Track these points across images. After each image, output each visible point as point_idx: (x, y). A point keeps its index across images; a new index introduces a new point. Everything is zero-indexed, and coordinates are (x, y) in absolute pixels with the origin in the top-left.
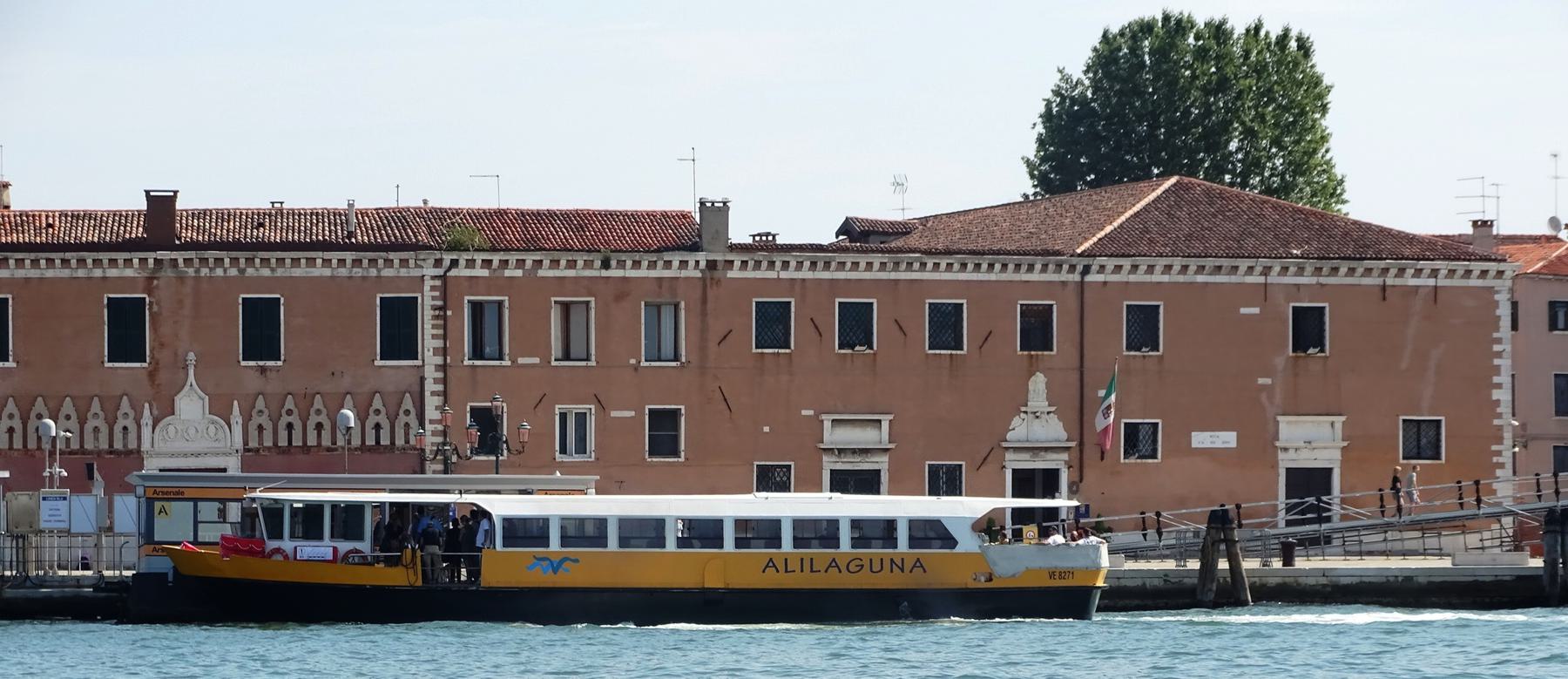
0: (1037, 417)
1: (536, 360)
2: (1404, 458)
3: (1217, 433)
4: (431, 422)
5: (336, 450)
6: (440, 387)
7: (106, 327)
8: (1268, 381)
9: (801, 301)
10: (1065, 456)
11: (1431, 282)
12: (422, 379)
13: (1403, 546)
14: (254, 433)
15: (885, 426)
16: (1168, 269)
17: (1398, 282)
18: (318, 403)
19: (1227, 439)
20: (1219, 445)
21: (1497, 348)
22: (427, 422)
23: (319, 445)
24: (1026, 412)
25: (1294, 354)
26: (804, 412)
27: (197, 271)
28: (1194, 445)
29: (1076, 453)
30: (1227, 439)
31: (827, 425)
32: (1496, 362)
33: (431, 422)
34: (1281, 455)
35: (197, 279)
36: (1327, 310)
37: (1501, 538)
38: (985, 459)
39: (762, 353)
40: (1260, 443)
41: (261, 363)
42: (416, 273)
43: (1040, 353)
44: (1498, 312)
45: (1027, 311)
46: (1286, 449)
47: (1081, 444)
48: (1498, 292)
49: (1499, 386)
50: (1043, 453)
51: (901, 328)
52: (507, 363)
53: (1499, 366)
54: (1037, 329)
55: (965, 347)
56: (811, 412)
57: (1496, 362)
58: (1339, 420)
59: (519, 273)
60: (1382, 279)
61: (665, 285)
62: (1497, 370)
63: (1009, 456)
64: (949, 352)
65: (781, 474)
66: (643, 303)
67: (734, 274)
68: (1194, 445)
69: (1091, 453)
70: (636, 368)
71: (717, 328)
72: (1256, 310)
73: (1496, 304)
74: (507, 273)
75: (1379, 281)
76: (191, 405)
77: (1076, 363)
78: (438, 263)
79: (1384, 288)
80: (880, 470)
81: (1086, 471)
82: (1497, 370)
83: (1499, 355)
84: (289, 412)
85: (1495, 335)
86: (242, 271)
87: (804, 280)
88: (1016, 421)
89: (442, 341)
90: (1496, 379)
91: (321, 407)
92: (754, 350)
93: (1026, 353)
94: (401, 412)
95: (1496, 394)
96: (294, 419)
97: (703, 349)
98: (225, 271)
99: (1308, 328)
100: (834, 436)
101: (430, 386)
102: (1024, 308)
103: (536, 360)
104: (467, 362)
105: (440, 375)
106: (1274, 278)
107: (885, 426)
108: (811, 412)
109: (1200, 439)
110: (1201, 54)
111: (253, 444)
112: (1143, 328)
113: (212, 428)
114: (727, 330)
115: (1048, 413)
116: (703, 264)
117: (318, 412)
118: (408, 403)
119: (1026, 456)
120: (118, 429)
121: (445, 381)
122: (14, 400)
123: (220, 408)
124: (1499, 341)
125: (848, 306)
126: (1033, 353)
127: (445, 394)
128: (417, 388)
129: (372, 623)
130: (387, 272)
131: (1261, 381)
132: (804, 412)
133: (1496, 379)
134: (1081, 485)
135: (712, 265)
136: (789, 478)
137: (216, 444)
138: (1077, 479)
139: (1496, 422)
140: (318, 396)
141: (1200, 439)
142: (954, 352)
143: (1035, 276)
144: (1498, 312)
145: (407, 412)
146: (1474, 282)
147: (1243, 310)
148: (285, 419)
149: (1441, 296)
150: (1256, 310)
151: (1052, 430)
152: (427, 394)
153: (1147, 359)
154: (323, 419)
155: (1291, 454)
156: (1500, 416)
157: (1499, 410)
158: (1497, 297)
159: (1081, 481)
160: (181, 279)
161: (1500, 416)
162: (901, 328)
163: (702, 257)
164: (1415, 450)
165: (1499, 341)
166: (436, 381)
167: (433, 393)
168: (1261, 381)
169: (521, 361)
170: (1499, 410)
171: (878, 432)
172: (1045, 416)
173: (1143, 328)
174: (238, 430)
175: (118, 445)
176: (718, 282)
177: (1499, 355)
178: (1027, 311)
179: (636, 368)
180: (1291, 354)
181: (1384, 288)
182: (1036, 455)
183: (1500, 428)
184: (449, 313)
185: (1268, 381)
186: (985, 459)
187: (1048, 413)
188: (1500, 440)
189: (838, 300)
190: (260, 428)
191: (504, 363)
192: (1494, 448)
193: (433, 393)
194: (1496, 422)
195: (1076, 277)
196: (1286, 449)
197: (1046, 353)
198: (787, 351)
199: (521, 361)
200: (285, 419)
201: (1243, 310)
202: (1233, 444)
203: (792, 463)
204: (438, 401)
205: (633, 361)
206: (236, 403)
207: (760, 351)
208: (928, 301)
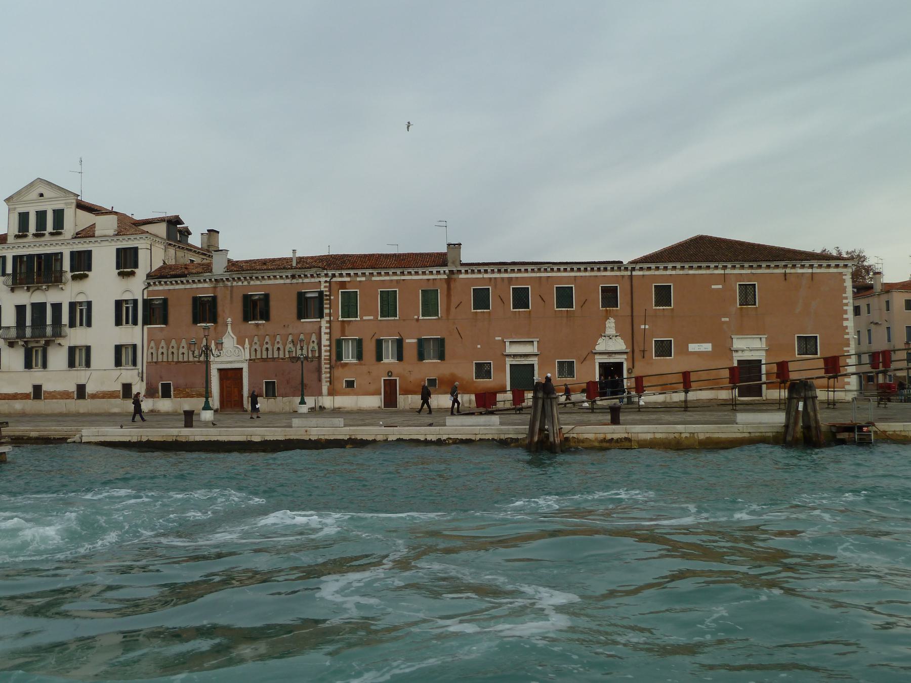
0: (610, 338)
1: (372, 318)
2: (798, 354)
3: (701, 344)
4: (324, 346)
5: (285, 359)
6: (328, 331)
7: (379, 296)
8: (727, 319)
9: (495, 286)
10: (625, 356)
11: (810, 271)
12: (320, 327)
13: (671, 398)
14: (253, 353)
15: (536, 344)
16: (674, 268)
17: (793, 271)
18: (278, 339)
19: (707, 347)
20: (702, 349)
21: (845, 301)
22: (322, 346)
23: (267, 358)
24: (605, 336)
25: (740, 307)
26: (497, 338)
27: (232, 283)
28: (690, 350)
29: (630, 355)
30: (707, 347)
31: (507, 344)
32: (845, 308)
33: (324, 346)
34: (734, 354)
35: (232, 287)
36: (756, 285)
37: (834, 391)
38: (585, 359)
39: (476, 312)
40: (724, 348)
41: (256, 322)
42: (317, 280)
43: (611, 309)
44: (845, 284)
45: (604, 290)
46: (737, 351)
47: (633, 351)
48: (846, 275)
49: (847, 319)
50: (614, 355)
51: (542, 299)
52: (358, 319)
53: (847, 310)
54: (610, 296)
55: (574, 307)
56: (500, 338)
57: (845, 308)
58: (764, 337)
59: (363, 279)
60: (784, 270)
61: (493, 280)
62: (846, 312)
63: (597, 357)
64: (566, 309)
65: (487, 367)
66: (420, 291)
67: (462, 276)
68: (690, 350)
69: (638, 355)
70: (418, 320)
71: (455, 300)
72: (720, 287)
73: (844, 281)
74: (358, 279)
75: (783, 271)
76: (229, 341)
77: (630, 314)
78: (326, 275)
79: (785, 274)
80: (534, 364)
81: (636, 364)
82: (846, 312)
83: (847, 305)
84: (152, 348)
85: (844, 295)
86: (249, 283)
87: (495, 278)
88: (600, 341)
89: (329, 310)
90: (845, 316)
91: (257, 342)
92: (472, 311)
93: (604, 309)
94: (311, 342)
95: (845, 323)
96: (269, 346)
97: (448, 309)
98: (242, 283)
99: (748, 293)
100: (511, 349)
101: (324, 330)
102: (603, 288)
103: (372, 318)
104: (340, 319)
105: (328, 325)
106: (728, 271)
107: (536, 344)
108: (500, 338)
109: (693, 347)
110: (180, 231)
111: (253, 357)
112: (663, 295)
113: (237, 351)
114: (460, 302)
115: (616, 336)
116: (447, 272)
117: (267, 343)
118: (314, 338)
119: (605, 357)
120: (275, 349)
121: (330, 328)
122: (176, 340)
123: (241, 342)
124: (846, 298)
125: (520, 289)
126: (608, 309)
127: (330, 333)
128: (317, 331)
129: (205, 441)
130: (306, 280)
131: (723, 319)
132: (497, 338)
133: (845, 316)
134: (633, 370)
135: (451, 272)
136: (490, 368)
137: (238, 358)
138: (631, 367)
139: (846, 337)
140: (267, 336)
141: (693, 347)
142: (568, 309)
143: (608, 273)
144: (845, 284)
145: (162, 347)
146: (832, 270)
147: (713, 287)
148: (265, 346)
149: (788, 276)
150: (720, 287)
151: (619, 345)
152: (323, 334)
153: (261, 327)
154: (280, 346)
155: (740, 353)
156: (848, 334)
157: (847, 331)
158: (844, 277)
159: (633, 368)
160: (226, 286)
161: (848, 334)
162: (542, 299)
163: (447, 269)
164: (805, 352)
165: (846, 298)
166: (327, 328)
167: (326, 333)
168: (723, 319)
169: (365, 318)
170: (847, 331)
171: (532, 347)
172: (614, 338)
173: (663, 295)
174: (247, 351)
175: (170, 360)
176: (455, 280)
177: (847, 305)
178: (604, 290)
179: (418, 320)
180: (738, 306)
181: (785, 274)
182: (610, 356)
183: (848, 339)
184: (332, 298)
185: (727, 319)
186: (585, 359)
187: (616, 336)
188: (848, 345)
189: (511, 287)
190: (256, 350)
191: (357, 319)
192: (845, 349)
193: (326, 333)
194: (846, 337)
195: (629, 273)
196: (737, 351)
197: (614, 309)
198: (488, 310)
199: (365, 318)
200: (265, 346)
201: (713, 287)
202: (710, 349)
203: (492, 362)
204: (327, 336)
205: (416, 317)
206: (247, 340)
207: (475, 311)
208: (555, 286)
